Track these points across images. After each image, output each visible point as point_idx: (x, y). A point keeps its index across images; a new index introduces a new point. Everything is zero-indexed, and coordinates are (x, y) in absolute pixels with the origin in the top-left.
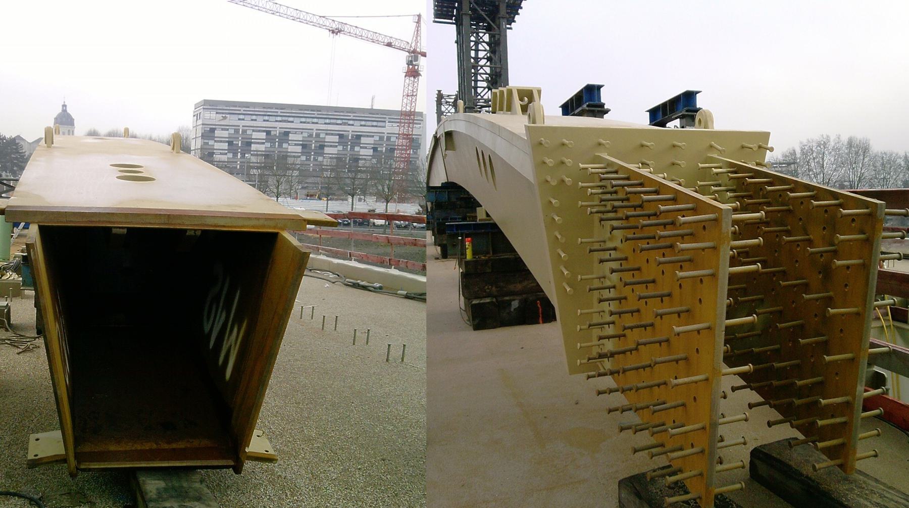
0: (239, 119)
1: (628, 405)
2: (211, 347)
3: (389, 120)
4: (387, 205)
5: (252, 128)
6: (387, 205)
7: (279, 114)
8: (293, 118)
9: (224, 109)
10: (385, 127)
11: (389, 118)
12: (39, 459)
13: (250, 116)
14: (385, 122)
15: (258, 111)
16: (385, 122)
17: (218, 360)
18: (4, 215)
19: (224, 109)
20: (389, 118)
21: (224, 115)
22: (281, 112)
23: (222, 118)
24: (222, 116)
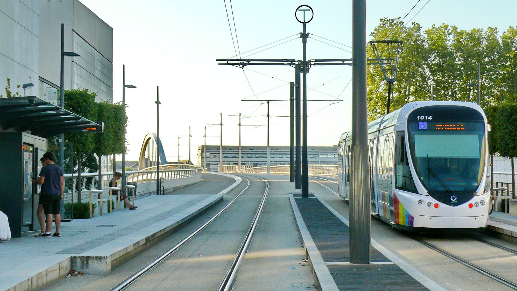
0: (248, 157)
1: (72, 163)
2: (61, 117)
3: (321, 153)
4: (147, 176)
5: (280, 163)
6: (147, 176)
7: (250, 152)
8: (251, 155)
9: (264, 152)
10: (266, 157)
11: (321, 152)
12: (37, 189)
13: (255, 155)
14: (318, 154)
15: (255, 151)
16: (318, 154)
17: (62, 116)
18: (12, 237)
19: (264, 152)
20: (321, 152)
21: (215, 155)
22: (251, 151)
23: (213, 157)
24: (214, 155)
